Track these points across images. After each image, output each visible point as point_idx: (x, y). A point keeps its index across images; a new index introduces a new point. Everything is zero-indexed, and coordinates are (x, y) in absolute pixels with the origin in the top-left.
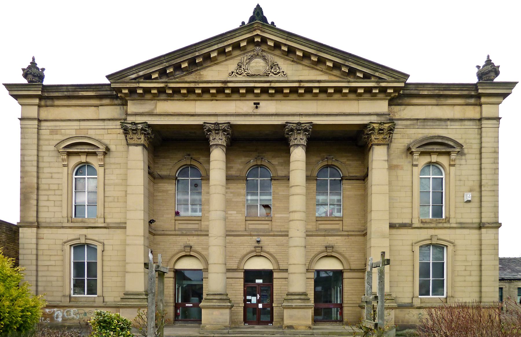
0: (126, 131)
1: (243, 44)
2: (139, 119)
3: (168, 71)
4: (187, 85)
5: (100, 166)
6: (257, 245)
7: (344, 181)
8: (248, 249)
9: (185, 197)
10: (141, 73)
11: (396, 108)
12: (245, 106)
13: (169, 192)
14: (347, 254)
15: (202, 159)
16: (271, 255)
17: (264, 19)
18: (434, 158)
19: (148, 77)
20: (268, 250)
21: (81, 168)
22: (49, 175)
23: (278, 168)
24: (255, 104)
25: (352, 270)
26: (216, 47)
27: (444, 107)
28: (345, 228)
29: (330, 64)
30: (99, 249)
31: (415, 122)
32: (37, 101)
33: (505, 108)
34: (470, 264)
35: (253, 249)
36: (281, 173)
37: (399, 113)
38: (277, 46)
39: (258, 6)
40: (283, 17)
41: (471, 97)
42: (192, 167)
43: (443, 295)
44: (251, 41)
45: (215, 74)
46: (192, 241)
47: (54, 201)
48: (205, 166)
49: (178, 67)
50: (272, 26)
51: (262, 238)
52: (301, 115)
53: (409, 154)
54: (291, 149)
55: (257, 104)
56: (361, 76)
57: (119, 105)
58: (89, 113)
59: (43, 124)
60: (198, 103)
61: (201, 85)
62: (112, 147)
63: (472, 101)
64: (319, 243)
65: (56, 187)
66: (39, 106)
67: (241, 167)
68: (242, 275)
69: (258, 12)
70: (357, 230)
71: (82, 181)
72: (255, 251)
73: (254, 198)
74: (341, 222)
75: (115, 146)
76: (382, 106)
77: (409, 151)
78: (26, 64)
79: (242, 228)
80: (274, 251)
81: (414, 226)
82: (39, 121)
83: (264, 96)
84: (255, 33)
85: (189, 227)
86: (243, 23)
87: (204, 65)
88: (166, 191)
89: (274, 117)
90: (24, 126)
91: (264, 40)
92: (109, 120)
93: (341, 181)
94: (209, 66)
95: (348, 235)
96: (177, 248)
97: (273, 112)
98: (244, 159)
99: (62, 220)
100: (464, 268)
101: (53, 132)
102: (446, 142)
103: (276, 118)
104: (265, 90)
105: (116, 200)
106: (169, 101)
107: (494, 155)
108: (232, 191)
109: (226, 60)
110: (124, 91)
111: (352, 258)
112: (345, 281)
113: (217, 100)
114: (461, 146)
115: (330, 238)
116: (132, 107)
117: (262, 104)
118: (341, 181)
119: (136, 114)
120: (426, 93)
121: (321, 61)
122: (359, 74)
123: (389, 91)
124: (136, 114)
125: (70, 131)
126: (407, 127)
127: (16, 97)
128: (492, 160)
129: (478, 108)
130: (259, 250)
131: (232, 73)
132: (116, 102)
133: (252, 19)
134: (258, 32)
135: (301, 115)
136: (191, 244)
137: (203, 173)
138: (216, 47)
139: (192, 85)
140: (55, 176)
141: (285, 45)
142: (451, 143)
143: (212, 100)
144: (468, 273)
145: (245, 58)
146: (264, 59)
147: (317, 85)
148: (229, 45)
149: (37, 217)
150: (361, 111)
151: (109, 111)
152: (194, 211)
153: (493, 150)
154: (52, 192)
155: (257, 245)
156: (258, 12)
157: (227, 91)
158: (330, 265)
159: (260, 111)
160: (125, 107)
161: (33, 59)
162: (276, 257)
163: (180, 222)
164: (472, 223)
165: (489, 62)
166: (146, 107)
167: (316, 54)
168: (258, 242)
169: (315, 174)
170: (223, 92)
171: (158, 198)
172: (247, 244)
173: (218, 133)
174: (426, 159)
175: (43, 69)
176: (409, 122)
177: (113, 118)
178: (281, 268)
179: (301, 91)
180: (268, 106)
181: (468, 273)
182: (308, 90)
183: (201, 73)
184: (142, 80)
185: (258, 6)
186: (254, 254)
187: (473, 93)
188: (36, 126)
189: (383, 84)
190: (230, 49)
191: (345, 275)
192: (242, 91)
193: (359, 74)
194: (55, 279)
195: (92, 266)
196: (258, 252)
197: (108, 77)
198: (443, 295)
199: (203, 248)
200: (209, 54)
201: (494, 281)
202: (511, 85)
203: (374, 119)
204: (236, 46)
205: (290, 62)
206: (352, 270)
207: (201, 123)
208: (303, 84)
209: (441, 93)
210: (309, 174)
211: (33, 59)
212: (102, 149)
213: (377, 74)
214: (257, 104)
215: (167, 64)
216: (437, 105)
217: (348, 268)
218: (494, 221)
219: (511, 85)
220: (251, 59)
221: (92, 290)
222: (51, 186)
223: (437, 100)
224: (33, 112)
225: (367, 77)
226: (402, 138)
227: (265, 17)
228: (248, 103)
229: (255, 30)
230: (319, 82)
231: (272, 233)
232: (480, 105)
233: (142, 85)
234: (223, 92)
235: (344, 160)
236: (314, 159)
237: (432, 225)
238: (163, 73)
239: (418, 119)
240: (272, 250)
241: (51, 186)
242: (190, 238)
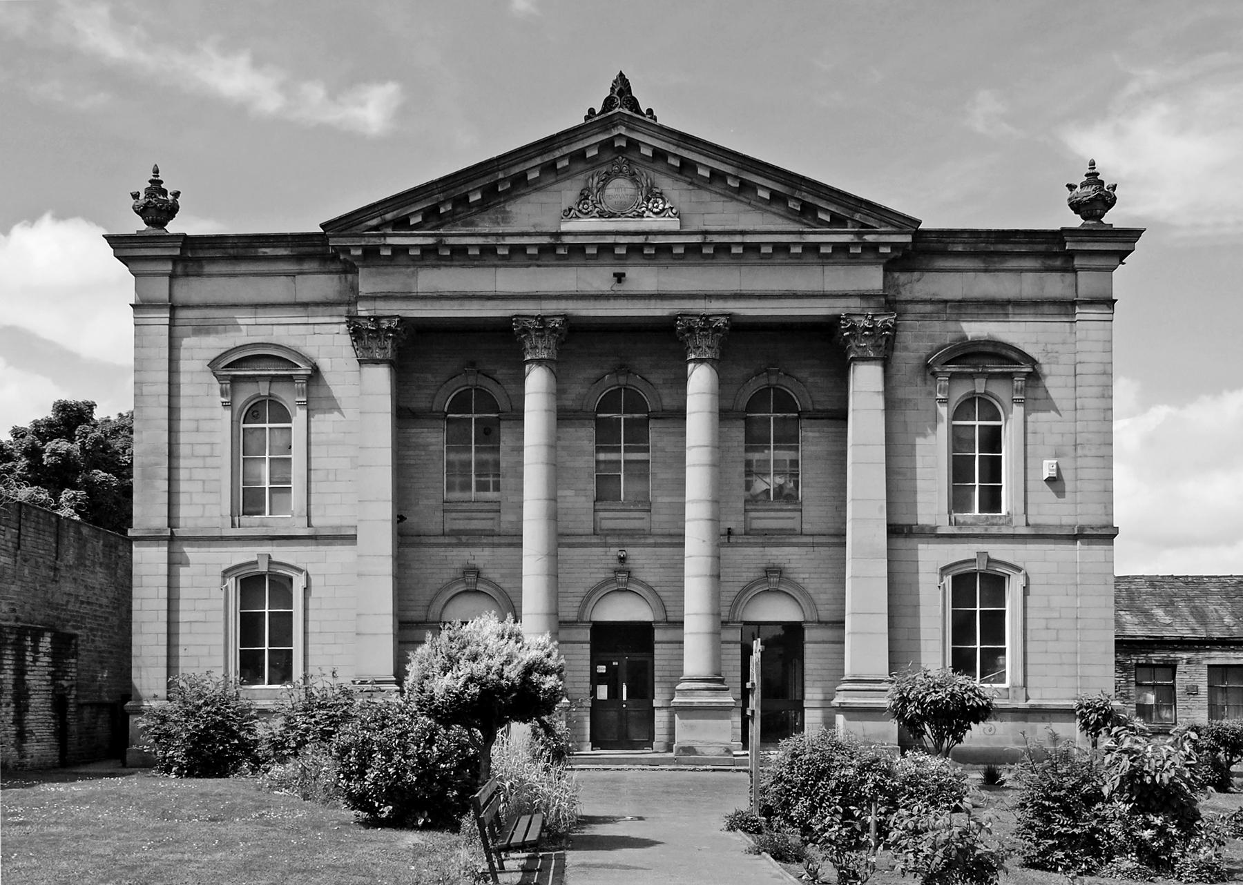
0: (357, 333)
1: (591, 153)
2: (384, 308)
3: (442, 211)
4: (480, 241)
5: (300, 404)
6: (619, 566)
7: (803, 423)
8: (601, 576)
9: (464, 457)
10: (389, 216)
11: (902, 277)
12: (598, 278)
13: (432, 448)
14: (812, 586)
15: (501, 373)
16: (649, 588)
17: (634, 104)
18: (980, 386)
19: (401, 224)
20: (643, 579)
21: (254, 412)
22: (193, 425)
23: (665, 392)
24: (615, 275)
25: (821, 623)
26: (538, 161)
27: (1002, 274)
28: (807, 528)
29: (765, 195)
30: (299, 583)
31: (941, 306)
32: (168, 267)
33: (1123, 279)
34: (1056, 615)
35: (612, 575)
36: (668, 402)
37: (908, 287)
38: (659, 155)
39: (621, 74)
40: (671, 106)
41: (1055, 255)
42: (481, 392)
43: (1003, 681)
44: (606, 146)
45: (533, 215)
46: (480, 556)
47: (204, 481)
48: (512, 388)
49: (461, 201)
50: (647, 119)
51: (631, 551)
52: (708, 297)
53: (929, 376)
54: (691, 366)
55: (620, 277)
56: (827, 218)
57: (337, 273)
58: (276, 289)
59: (182, 314)
60: (501, 271)
61: (509, 241)
62: (324, 364)
63: (1058, 263)
64: (749, 559)
65: (205, 450)
66: (172, 276)
67: (584, 391)
68: (586, 635)
69: (622, 87)
70: (832, 531)
71: (257, 434)
72: (614, 580)
73: (612, 456)
74: (797, 514)
75: (328, 361)
76: (872, 278)
77: (928, 370)
78: (142, 186)
79: (588, 527)
80: (657, 579)
81: (939, 532)
82: (173, 308)
83: (636, 259)
84: (615, 132)
85: (473, 527)
86: (592, 111)
87: (514, 194)
88: (425, 447)
89: (653, 302)
90: (140, 321)
91: (633, 145)
92: (317, 304)
93: (798, 418)
94: (524, 195)
95: (813, 545)
96: (448, 574)
97: (652, 291)
98: (593, 373)
99: (217, 522)
100: (1043, 623)
101: (202, 329)
102: (1004, 352)
103: (659, 304)
104: (634, 249)
105: (331, 477)
106: (443, 269)
107: (1103, 379)
108: (567, 443)
109: (557, 182)
110: (353, 252)
111: (822, 596)
112: (809, 649)
113: (539, 266)
114: (1032, 361)
115: (774, 551)
116: (367, 282)
117: (631, 273)
118: (798, 418)
119: (373, 297)
120: (960, 248)
121: (746, 188)
122: (821, 216)
123: (882, 250)
124: (373, 297)
125: (250, 331)
126: (924, 316)
127: (125, 260)
128: (1096, 391)
129: (1069, 277)
130: (622, 577)
131: (570, 210)
132: (332, 267)
133: (609, 103)
134: (622, 130)
135: (708, 297)
136: (479, 563)
137: (503, 404)
138: (538, 161)
139: (491, 241)
140: (205, 426)
141: (675, 156)
142: (1014, 355)
143: (529, 266)
144: (1052, 634)
145: (596, 179)
146: (633, 178)
147: (738, 239)
148: (563, 157)
149: (171, 516)
150: (830, 287)
151: (320, 285)
152: (482, 487)
153: (1100, 368)
154: (199, 462)
155: (619, 566)
156: (622, 87)
157: (561, 251)
158: (778, 611)
159: (626, 287)
160: (350, 277)
161: (156, 172)
162: (661, 594)
163: (454, 515)
164: (1061, 526)
165: (1093, 177)
166: (391, 281)
167: (740, 175)
168: (622, 560)
169: (743, 404)
170: (555, 251)
171: (412, 462)
172: (594, 563)
173: (542, 337)
174: (961, 391)
175: (177, 194)
176: (929, 308)
177: (324, 300)
178: (670, 619)
179: (708, 250)
180: (643, 278)
181: (1052, 634)
182: (723, 249)
183: (508, 209)
184: (389, 231)
185: (621, 74)
186: (614, 587)
187: (1056, 249)
188: (167, 321)
189: (869, 238)
190: (566, 163)
191: (809, 634)
192: (591, 251)
193: (821, 216)
194: (205, 650)
195: (283, 625)
196: (622, 579)
197: (321, 226)
198: (1003, 681)
199: (502, 576)
200: (524, 175)
201: (1106, 653)
202: (1132, 235)
203: (854, 305)
204: (580, 156)
205: (685, 186)
206: (821, 623)
207: (508, 314)
208: (710, 238)
209: (992, 247)
210: (728, 404)
211: (156, 172)
212: (304, 370)
213: (857, 217)
214: (620, 277)
215: (441, 197)
216: (986, 271)
217: (815, 618)
218: (1105, 523)
219: (1132, 235)
220: (608, 177)
221: (283, 672)
222: (197, 448)
223: (984, 262)
224: (159, 288)
225: (838, 221)
226: (921, 338)
227: (635, 99)
228: (600, 270)
229: (615, 126)
230: (743, 233)
231: (650, 541)
232: (1075, 271)
233: (390, 241)
234: (555, 251)
235: (803, 374)
236: (738, 372)
237: (977, 531)
238: (431, 214)
239: (946, 302)
240: (651, 579)
241: (197, 448)
242: (476, 552)
